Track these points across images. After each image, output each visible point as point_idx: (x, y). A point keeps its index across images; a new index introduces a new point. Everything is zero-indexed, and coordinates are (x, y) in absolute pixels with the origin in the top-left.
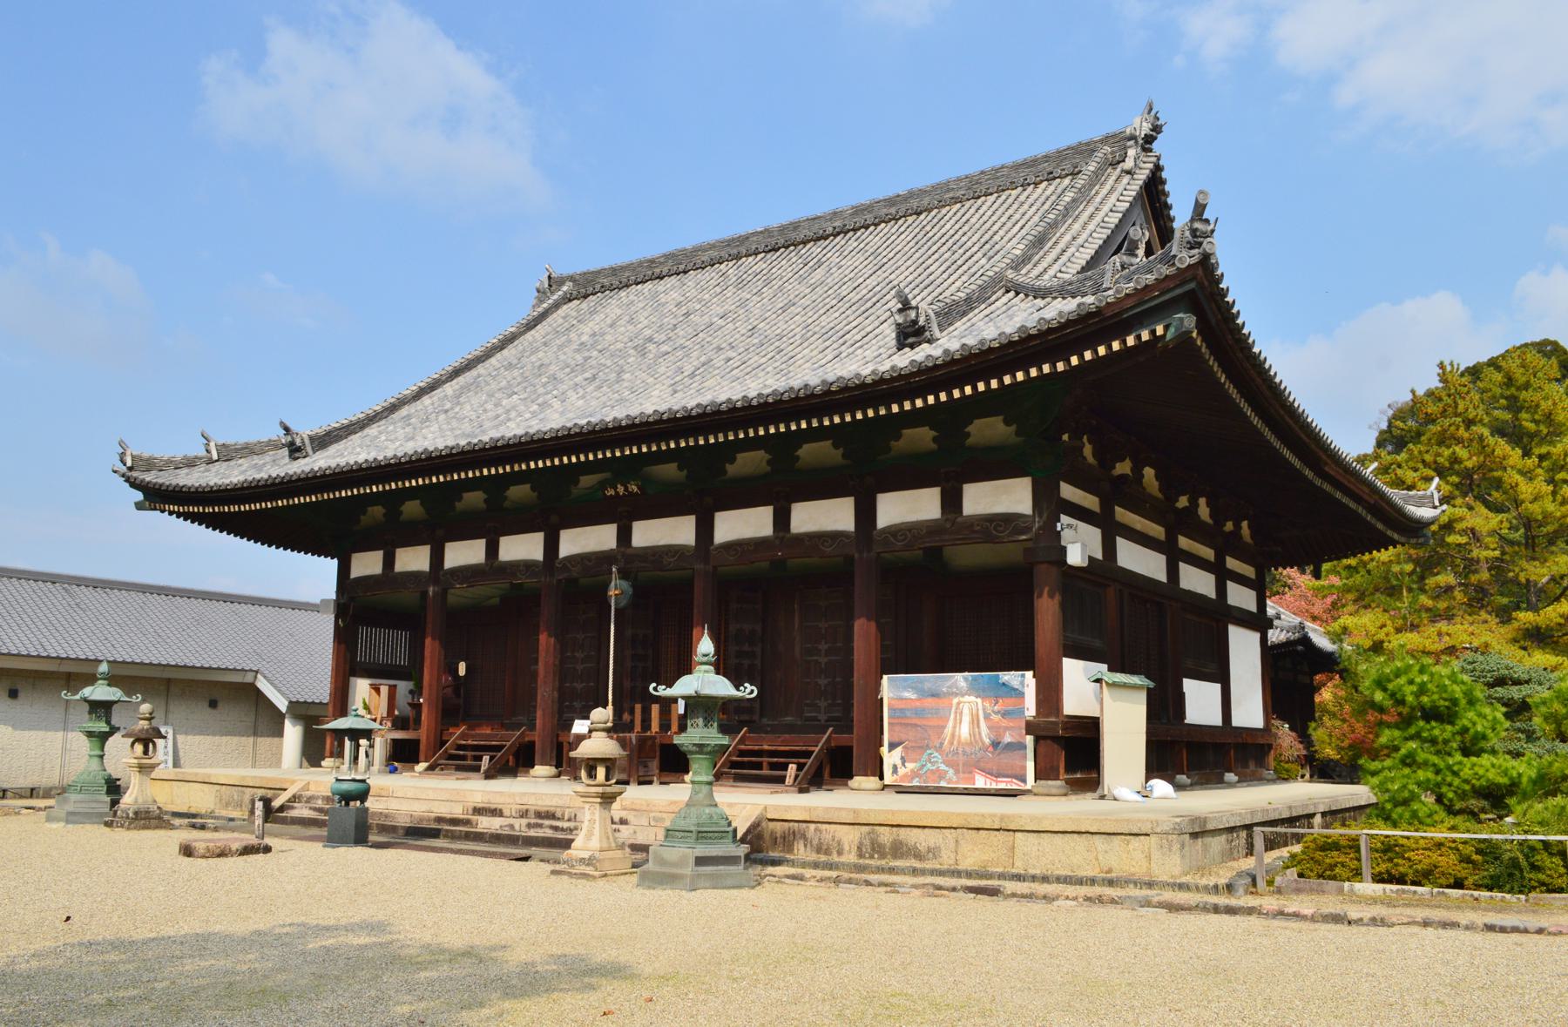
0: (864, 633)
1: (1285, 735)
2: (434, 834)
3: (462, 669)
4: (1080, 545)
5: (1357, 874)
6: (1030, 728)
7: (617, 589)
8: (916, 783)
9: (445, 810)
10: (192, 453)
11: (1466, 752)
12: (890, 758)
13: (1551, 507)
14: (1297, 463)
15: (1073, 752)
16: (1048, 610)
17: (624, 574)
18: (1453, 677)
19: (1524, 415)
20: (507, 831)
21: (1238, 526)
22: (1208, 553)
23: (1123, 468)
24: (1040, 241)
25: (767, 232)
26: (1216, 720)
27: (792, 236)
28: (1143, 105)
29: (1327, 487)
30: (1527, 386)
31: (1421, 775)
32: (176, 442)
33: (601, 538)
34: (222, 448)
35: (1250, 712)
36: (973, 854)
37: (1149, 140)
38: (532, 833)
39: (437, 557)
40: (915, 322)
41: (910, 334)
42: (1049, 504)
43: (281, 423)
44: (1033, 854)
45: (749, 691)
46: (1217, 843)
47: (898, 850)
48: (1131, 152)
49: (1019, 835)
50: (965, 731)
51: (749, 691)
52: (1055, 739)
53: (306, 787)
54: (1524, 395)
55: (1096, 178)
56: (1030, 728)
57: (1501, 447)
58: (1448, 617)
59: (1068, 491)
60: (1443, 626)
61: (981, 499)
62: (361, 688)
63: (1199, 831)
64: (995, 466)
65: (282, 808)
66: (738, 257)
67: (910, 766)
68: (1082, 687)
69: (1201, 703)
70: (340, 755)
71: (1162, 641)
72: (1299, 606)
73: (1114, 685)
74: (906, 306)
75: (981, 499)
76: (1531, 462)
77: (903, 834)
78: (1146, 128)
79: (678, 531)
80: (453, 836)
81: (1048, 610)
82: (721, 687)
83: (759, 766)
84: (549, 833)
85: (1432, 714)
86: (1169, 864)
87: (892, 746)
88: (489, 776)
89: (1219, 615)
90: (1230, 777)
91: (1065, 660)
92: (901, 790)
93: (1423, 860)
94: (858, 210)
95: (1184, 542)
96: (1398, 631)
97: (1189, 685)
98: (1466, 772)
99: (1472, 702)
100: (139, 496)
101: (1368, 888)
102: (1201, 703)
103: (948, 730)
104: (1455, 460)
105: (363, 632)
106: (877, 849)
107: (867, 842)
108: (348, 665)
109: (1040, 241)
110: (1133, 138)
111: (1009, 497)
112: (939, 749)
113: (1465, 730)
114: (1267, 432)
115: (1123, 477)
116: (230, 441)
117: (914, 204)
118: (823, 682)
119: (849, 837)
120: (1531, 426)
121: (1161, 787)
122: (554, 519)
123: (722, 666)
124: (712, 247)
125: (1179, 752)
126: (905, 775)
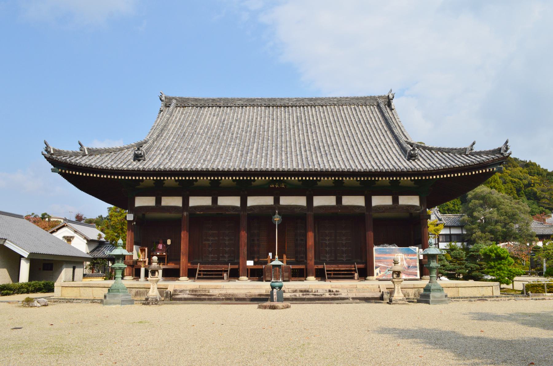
0: (370, 235)
3: (169, 242)
5: (545, 292)
7: (277, 219)
8: (384, 278)
17: (279, 214)
20: (294, 297)
27: (298, 104)
32: (66, 145)
38: (304, 297)
40: (141, 154)
43: (507, 142)
64: (408, 192)
67: (382, 273)
75: (404, 200)
83: (334, 274)
87: (376, 268)
107: (417, 293)
111: (414, 201)
118: (328, 249)
126: (381, 276)
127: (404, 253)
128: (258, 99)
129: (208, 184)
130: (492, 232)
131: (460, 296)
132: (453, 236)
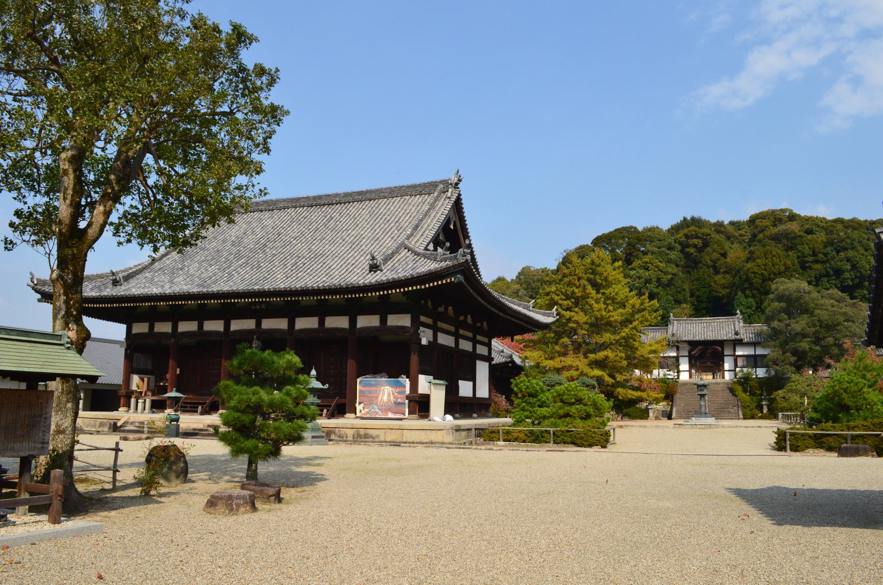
0: (351, 365)
1: (502, 400)
2: (196, 434)
5: (499, 440)
6: (407, 397)
9: (195, 426)
11: (540, 406)
12: (359, 407)
13: (604, 313)
14: (496, 312)
15: (420, 405)
16: (414, 360)
17: (258, 339)
18: (537, 384)
19: (597, 277)
21: (482, 324)
22: (470, 335)
23: (441, 309)
24: (416, 227)
25: (308, 198)
26: (470, 395)
27: (319, 202)
28: (455, 172)
29: (508, 317)
30: (599, 265)
31: (526, 413)
35: (483, 392)
36: (391, 436)
37: (457, 184)
39: (175, 327)
41: (374, 268)
44: (408, 436)
45: (326, 386)
46: (464, 434)
47: (366, 436)
48: (450, 190)
50: (385, 398)
51: (326, 386)
52: (416, 401)
53: (129, 418)
54: (599, 269)
55: (437, 199)
56: (407, 397)
57: (590, 289)
58: (565, 354)
59: (423, 319)
60: (563, 359)
61: (394, 320)
62: (136, 378)
63: (458, 429)
64: (399, 310)
65: (121, 427)
66: (296, 207)
67: (366, 410)
68: (424, 383)
69: (465, 389)
70: (129, 407)
71: (452, 367)
72: (501, 349)
73: (435, 384)
74: (373, 258)
75: (394, 320)
76: (600, 296)
78: (456, 180)
79: (282, 324)
80: (203, 435)
81: (414, 360)
82: (317, 385)
85: (531, 395)
86: (449, 438)
87: (360, 403)
88: (202, 414)
90: (475, 415)
92: (362, 418)
93: (516, 435)
94: (346, 195)
95: (461, 332)
96: (546, 359)
97: (461, 383)
98: (538, 413)
99: (543, 391)
100: (39, 296)
101: (501, 443)
102: (465, 389)
103: (380, 398)
104: (573, 293)
105: (136, 355)
106: (359, 436)
108: (131, 368)
109: (416, 227)
110: (451, 184)
111: (402, 320)
112: (376, 404)
113: (539, 400)
114: (486, 304)
115: (441, 313)
117: (368, 196)
119: (350, 433)
120: (600, 281)
121: (449, 417)
123: (318, 379)
124: (284, 200)
125: (456, 406)
127: (391, 386)
128: (303, 198)
129: (403, 299)
130: (795, 352)
131: (404, 440)
132: (759, 359)
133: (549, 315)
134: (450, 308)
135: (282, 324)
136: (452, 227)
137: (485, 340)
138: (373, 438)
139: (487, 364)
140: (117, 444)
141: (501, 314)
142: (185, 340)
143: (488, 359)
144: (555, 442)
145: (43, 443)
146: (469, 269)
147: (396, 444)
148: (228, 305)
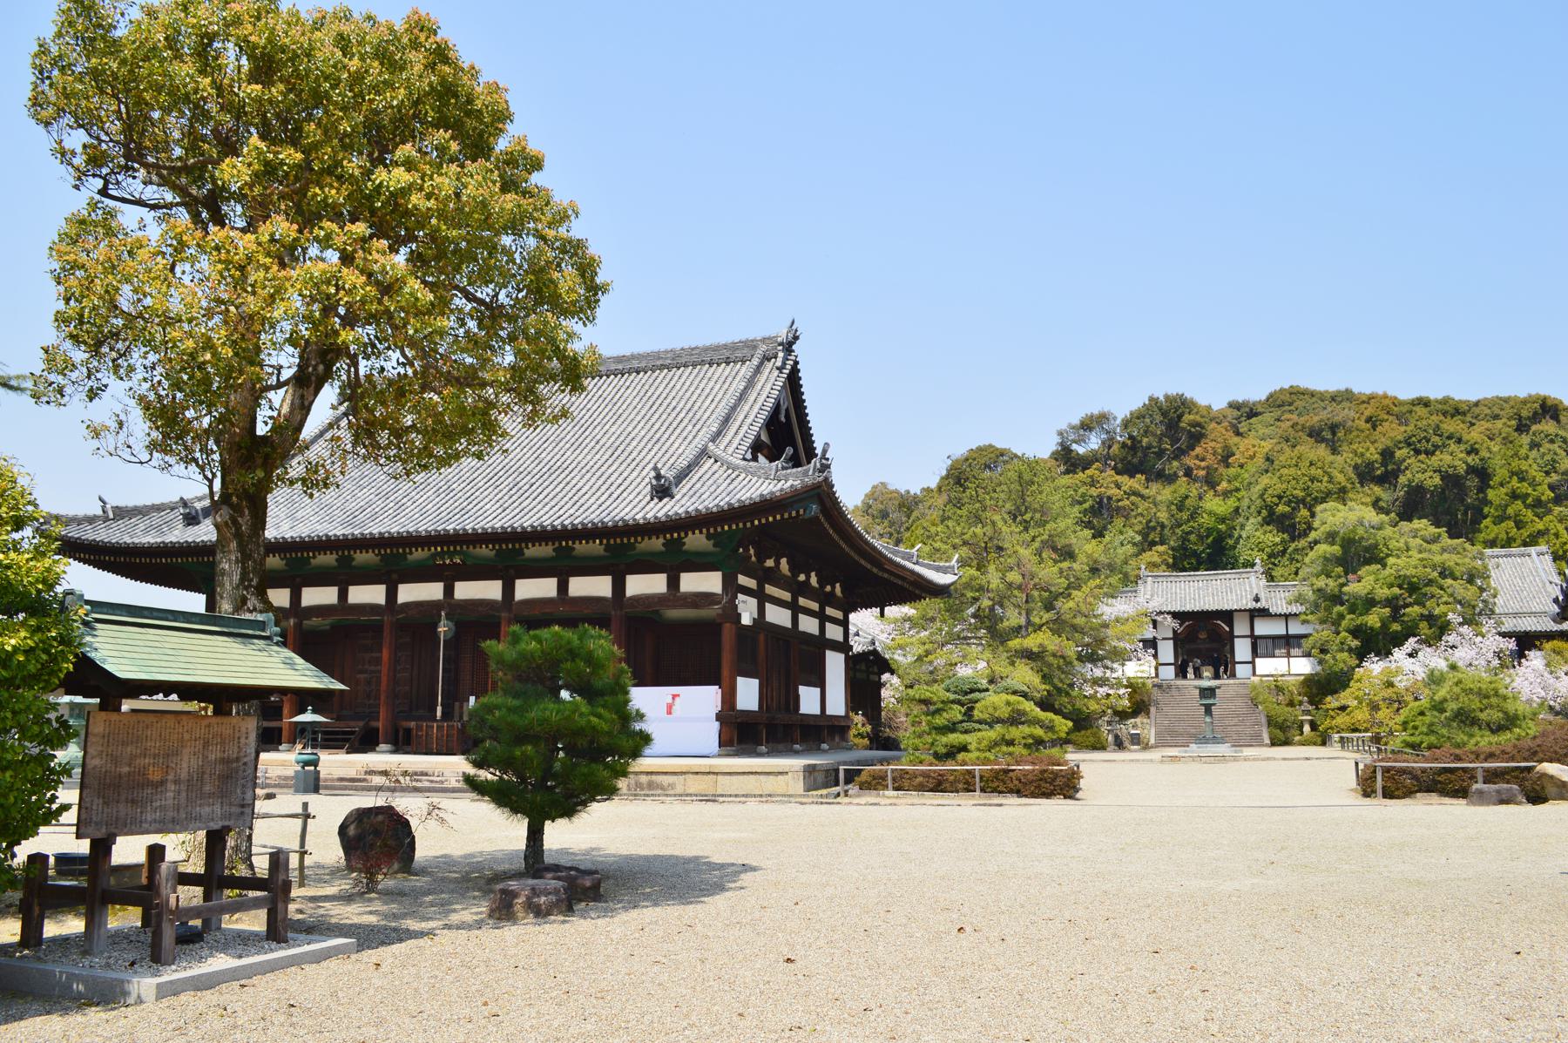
4: (747, 611)
5: (886, 787)
7: (443, 628)
10: (90, 513)
23: (770, 563)
26: (817, 711)
33: (432, 591)
34: (116, 509)
35: (837, 704)
37: (791, 344)
41: (662, 491)
42: (731, 586)
47: (651, 785)
49: (720, 777)
59: (743, 580)
64: (700, 564)
72: (869, 627)
74: (658, 477)
75: (692, 582)
77: (654, 777)
79: (490, 590)
84: (427, 784)
89: (821, 644)
90: (825, 746)
91: (740, 679)
97: (802, 690)
101: (891, 793)
109: (726, 420)
111: (707, 582)
116: (121, 504)
117: (635, 364)
122: (395, 576)
131: (719, 791)
133: (944, 570)
134: (784, 561)
135: (490, 590)
136: (783, 419)
137: (839, 615)
138: (662, 788)
139: (842, 657)
140: (305, 805)
141: (875, 570)
142: (315, 621)
143: (844, 647)
144: (983, 790)
145: (243, 806)
146: (823, 494)
147: (711, 799)
148: (507, 552)
